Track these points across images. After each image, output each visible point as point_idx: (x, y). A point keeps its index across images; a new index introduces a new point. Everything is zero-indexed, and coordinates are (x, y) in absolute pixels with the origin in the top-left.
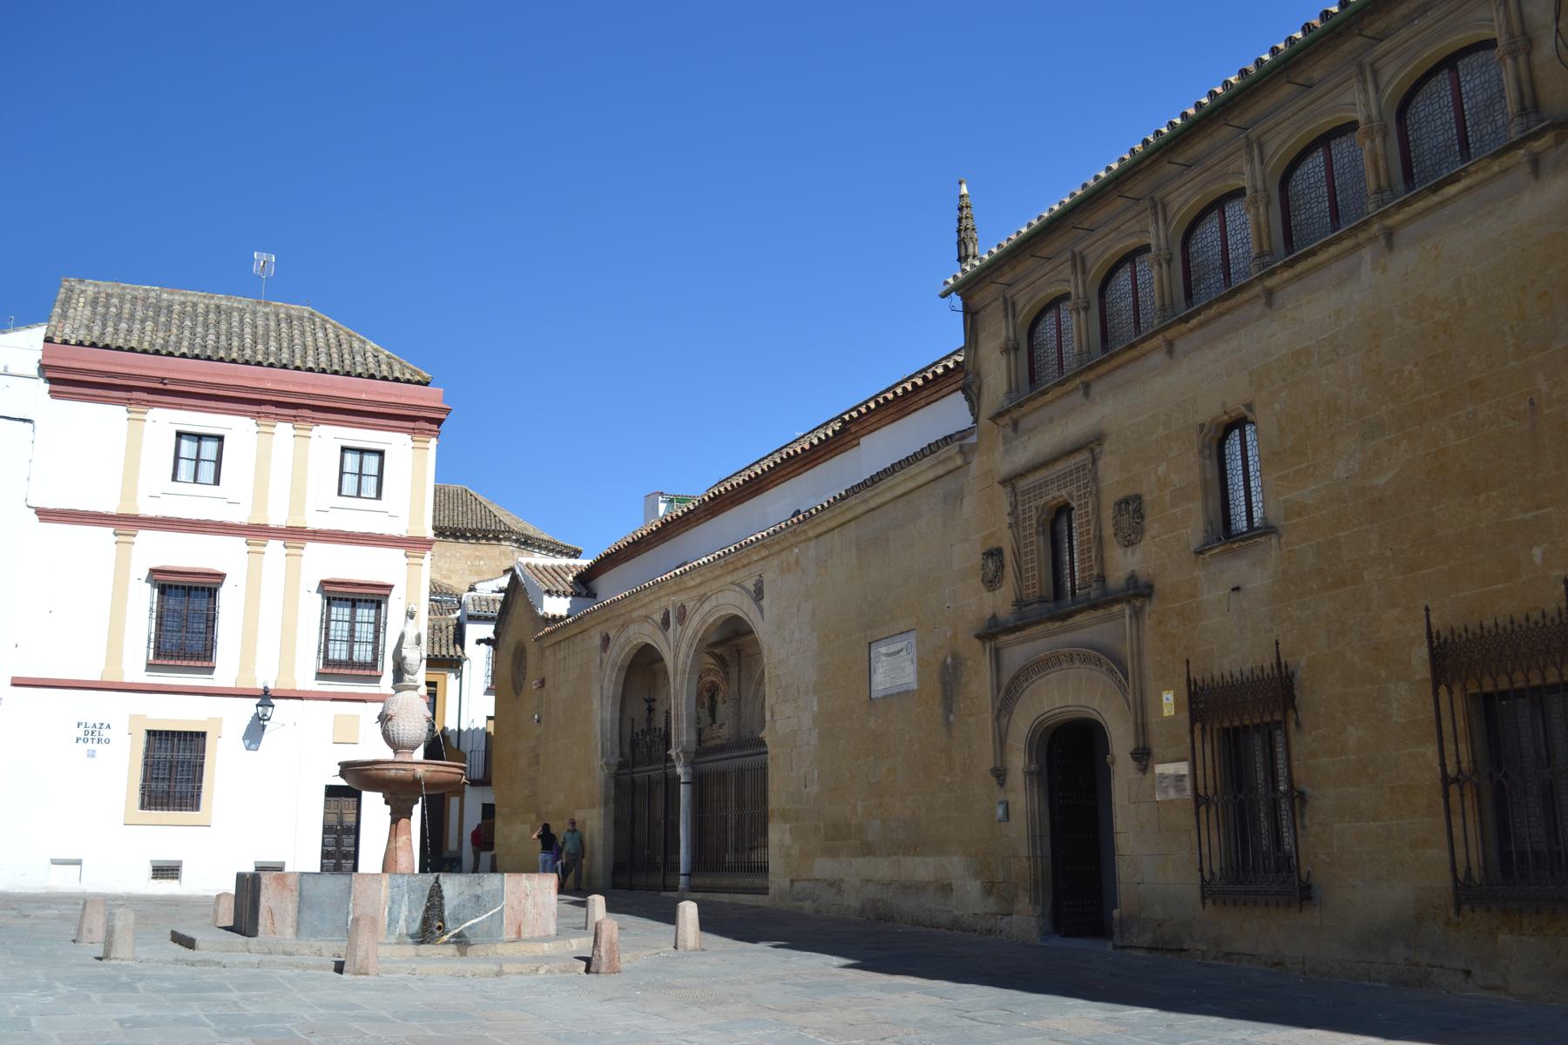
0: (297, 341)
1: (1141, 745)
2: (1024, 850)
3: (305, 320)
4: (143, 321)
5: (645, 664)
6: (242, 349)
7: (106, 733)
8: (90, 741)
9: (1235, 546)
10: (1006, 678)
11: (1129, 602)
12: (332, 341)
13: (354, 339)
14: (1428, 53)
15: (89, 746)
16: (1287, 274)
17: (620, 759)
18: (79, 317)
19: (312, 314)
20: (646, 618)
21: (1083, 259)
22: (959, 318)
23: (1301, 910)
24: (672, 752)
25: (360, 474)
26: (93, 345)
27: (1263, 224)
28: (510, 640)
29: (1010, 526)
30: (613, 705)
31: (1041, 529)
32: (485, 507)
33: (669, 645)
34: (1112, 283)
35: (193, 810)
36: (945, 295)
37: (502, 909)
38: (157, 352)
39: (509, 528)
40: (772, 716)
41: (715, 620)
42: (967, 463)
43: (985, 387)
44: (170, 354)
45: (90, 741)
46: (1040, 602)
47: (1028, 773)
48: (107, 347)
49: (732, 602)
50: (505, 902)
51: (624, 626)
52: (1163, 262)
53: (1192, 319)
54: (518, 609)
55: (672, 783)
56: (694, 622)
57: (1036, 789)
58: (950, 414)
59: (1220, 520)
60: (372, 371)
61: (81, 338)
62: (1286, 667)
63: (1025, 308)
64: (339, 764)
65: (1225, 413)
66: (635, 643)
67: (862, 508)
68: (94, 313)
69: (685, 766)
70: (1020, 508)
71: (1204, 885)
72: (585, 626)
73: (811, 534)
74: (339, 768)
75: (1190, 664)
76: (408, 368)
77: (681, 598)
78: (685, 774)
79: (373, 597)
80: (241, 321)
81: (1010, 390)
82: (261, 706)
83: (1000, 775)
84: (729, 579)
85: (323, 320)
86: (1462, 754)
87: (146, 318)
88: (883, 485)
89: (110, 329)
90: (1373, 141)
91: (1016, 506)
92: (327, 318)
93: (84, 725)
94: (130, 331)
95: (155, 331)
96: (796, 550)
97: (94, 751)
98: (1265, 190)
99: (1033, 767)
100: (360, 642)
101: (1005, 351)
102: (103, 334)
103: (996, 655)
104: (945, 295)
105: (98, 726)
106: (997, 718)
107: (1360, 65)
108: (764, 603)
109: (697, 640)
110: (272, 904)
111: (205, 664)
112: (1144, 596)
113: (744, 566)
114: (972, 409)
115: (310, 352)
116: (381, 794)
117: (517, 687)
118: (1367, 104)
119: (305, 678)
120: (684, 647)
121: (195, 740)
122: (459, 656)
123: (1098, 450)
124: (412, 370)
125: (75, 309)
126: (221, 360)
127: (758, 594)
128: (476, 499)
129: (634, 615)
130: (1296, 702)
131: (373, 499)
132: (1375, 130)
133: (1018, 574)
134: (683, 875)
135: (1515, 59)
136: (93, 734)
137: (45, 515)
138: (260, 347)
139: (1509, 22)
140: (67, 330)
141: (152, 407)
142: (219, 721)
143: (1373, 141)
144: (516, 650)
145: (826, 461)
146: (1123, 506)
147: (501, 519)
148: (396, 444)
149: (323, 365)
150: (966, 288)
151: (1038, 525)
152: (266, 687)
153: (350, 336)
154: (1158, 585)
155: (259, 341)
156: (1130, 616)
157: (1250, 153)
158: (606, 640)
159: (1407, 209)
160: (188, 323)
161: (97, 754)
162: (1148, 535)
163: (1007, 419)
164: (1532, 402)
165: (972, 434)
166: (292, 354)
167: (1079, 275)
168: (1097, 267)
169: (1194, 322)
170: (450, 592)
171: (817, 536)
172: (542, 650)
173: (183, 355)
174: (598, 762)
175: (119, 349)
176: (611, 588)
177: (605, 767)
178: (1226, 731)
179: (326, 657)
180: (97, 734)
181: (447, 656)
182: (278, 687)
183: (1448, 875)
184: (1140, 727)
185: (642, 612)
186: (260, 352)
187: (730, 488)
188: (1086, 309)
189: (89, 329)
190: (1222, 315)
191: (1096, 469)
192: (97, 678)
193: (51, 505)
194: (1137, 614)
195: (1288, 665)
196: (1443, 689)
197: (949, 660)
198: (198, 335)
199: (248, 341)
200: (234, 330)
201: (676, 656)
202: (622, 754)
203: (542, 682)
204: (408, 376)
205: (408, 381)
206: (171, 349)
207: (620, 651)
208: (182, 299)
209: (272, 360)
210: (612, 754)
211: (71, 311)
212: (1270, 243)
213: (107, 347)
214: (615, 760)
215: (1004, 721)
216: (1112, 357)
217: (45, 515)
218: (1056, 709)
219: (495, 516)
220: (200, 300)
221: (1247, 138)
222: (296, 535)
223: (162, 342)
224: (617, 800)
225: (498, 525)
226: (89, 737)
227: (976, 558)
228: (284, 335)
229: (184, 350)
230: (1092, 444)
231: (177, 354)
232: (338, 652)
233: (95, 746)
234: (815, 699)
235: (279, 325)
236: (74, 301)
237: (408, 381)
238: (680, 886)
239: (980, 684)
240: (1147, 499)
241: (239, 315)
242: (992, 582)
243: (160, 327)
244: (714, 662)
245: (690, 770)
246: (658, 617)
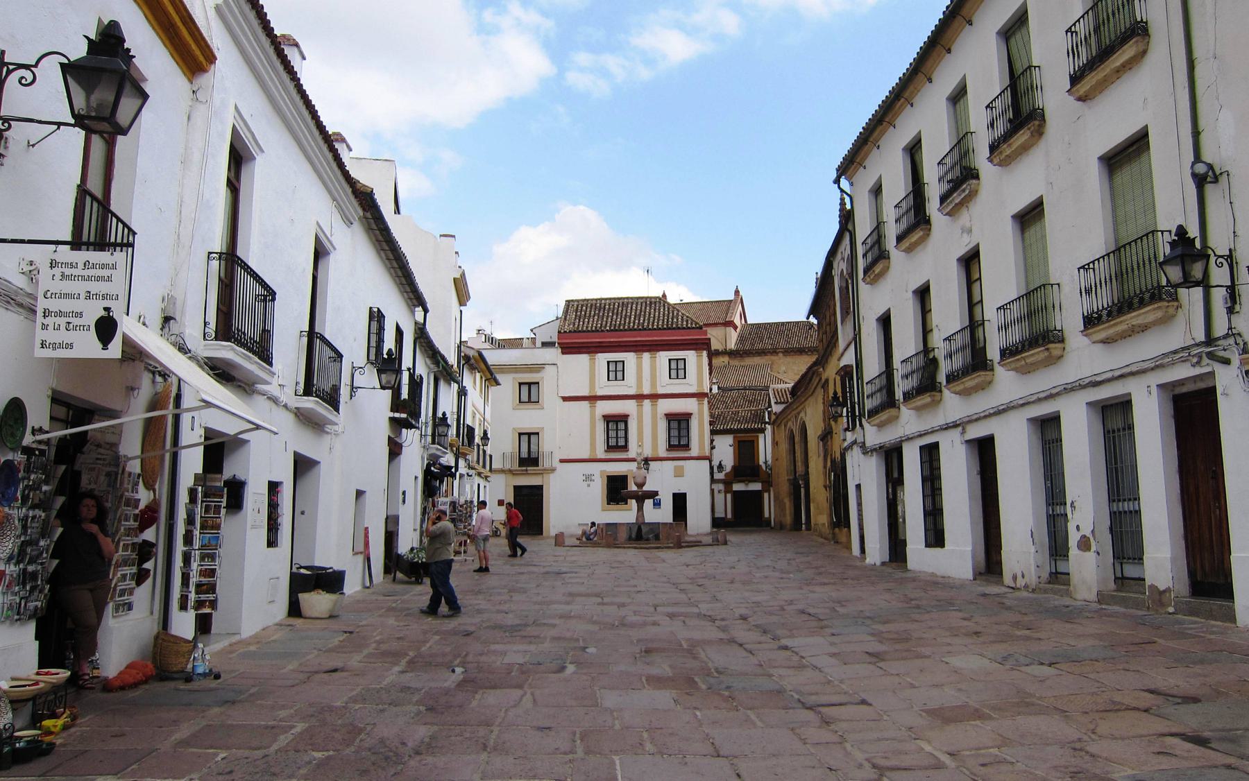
7: (593, 478)
15: (588, 482)
23: (235, 475)
25: (677, 369)
79: (623, 419)
95: (569, 325)
115: (656, 320)
119: (662, 452)
137: (565, 399)
148: (690, 356)
179: (608, 443)
192: (687, 461)
199: (680, 320)
217: (565, 399)
222: (654, 397)
232: (612, 442)
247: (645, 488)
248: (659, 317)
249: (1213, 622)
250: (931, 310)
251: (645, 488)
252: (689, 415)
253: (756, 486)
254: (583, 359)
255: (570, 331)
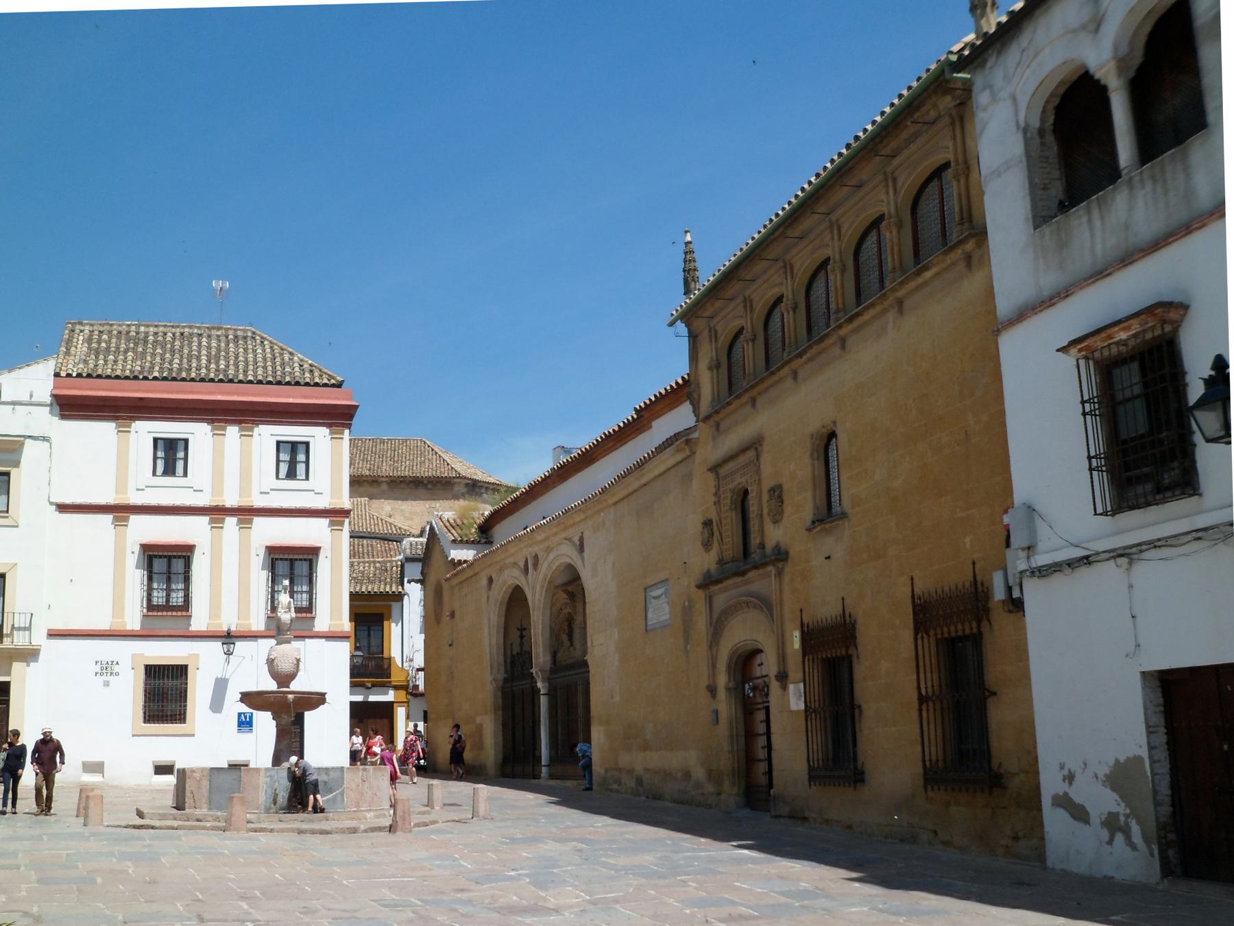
0: (241, 358)
1: (782, 669)
2: (726, 746)
3: (249, 339)
4: (126, 352)
5: (516, 600)
6: (198, 369)
7: (116, 668)
8: (105, 674)
9: (827, 526)
10: (715, 616)
11: (774, 565)
12: (269, 355)
13: (286, 352)
14: (921, 168)
15: (104, 678)
16: (850, 327)
17: (506, 676)
18: (78, 353)
19: (254, 333)
20: (515, 564)
21: (751, 301)
22: (684, 343)
24: (533, 671)
26: (89, 376)
27: (839, 288)
28: (432, 579)
29: (715, 503)
30: (498, 632)
31: (733, 506)
32: (440, 456)
33: (528, 585)
34: (771, 320)
35: (181, 723)
36: (671, 324)
37: (343, 790)
38: (136, 378)
39: (459, 474)
40: (592, 643)
41: (558, 567)
42: (693, 453)
43: (702, 395)
44: (145, 378)
45: (105, 674)
46: (733, 561)
47: (728, 689)
48: (99, 376)
49: (569, 553)
50: (345, 786)
51: (501, 570)
52: (790, 309)
53: (804, 355)
54: (436, 556)
55: (535, 692)
56: (544, 568)
57: (733, 701)
58: (681, 418)
59: (825, 506)
60: (297, 379)
61: (80, 371)
62: (850, 616)
63: (724, 337)
64: (240, 693)
65: (824, 427)
66: (509, 583)
67: (636, 485)
68: (89, 348)
69: (543, 682)
70: (721, 489)
71: (811, 769)
72: (476, 571)
73: (611, 502)
74: (240, 696)
75: (803, 612)
76: (326, 373)
77: (535, 549)
78: (543, 687)
80: (200, 343)
81: (713, 401)
82: (225, 644)
83: (712, 690)
84: (563, 535)
85: (262, 337)
86: (931, 682)
87: (128, 349)
88: (647, 467)
89: (101, 362)
90: (891, 232)
91: (719, 488)
92: (265, 336)
93: (100, 663)
94: (115, 362)
96: (602, 514)
97: (108, 682)
98: (841, 261)
99: (731, 685)
100: (302, 591)
101: (710, 369)
102: (96, 366)
103: (710, 600)
104: (671, 324)
105: (110, 663)
106: (711, 647)
107: (885, 173)
108: (586, 554)
109: (547, 582)
110: (192, 788)
111: (184, 613)
112: (782, 560)
113: (572, 526)
114: (694, 411)
115: (251, 367)
116: (270, 713)
117: (438, 619)
118: (889, 203)
120: (538, 589)
121: (179, 672)
122: (400, 592)
123: (759, 449)
124: (329, 375)
125: (76, 348)
126: (183, 380)
127: (581, 549)
128: (433, 450)
129: (507, 561)
130: (857, 641)
131: (303, 480)
132: (891, 224)
133: (720, 540)
134: (545, 766)
135: (959, 181)
136: (107, 669)
137: (63, 508)
138: (213, 366)
139: (956, 150)
140: (70, 366)
141: (134, 420)
142: (197, 656)
143: (891, 232)
144: (436, 588)
145: (633, 438)
146: (772, 492)
147: (453, 466)
148: (318, 436)
149: (260, 378)
150: (688, 316)
151: (732, 503)
152: (229, 630)
153: (282, 349)
154: (792, 553)
155: (212, 361)
156: (775, 575)
157: (832, 232)
158: (491, 580)
159: (906, 286)
160: (159, 351)
161: (111, 684)
162: (786, 514)
163: (711, 422)
164: (966, 434)
165: (696, 431)
166: (236, 370)
167: (748, 314)
168: (760, 308)
169: (805, 358)
170: (408, 533)
171: (616, 503)
172: (452, 588)
173: (155, 378)
174: (489, 678)
175: (108, 377)
176: (504, 532)
177: (493, 682)
178: (823, 660)
179: (149, 600)
180: (109, 669)
181: (390, 593)
182: (238, 629)
183: (920, 764)
184: (781, 656)
185: (511, 560)
186: (213, 370)
187: (570, 460)
188: (753, 340)
189: (86, 362)
190: (820, 353)
191: (760, 464)
193: (68, 501)
194: (780, 574)
195: (852, 615)
196: (919, 636)
197: (687, 603)
198: (166, 360)
200: (193, 353)
201: (534, 595)
202: (506, 672)
203: (452, 615)
204: (326, 381)
205: (325, 385)
206: (146, 374)
207: (500, 592)
208: (156, 330)
209: (221, 377)
210: (499, 670)
211: (73, 348)
212: (844, 303)
213: (99, 376)
214: (501, 676)
215: (714, 650)
216: (773, 373)
217: (63, 508)
218: (748, 640)
219: (448, 464)
220: (168, 329)
221: (830, 220)
222: (246, 513)
223: (139, 368)
224: (504, 708)
225: (450, 472)
226: (104, 671)
227: (700, 527)
228: (231, 354)
229: (156, 374)
230: (755, 445)
231: (150, 377)
233: (109, 678)
234: (616, 630)
235: (228, 345)
236: (75, 340)
237: (325, 385)
238: (542, 775)
239: (701, 623)
240: (785, 488)
241: (198, 340)
242: (707, 545)
243: (139, 356)
244: (567, 597)
245: (547, 685)
246: (522, 564)
247: (295, 686)
248: (256, 362)
249: (723, 852)
250: (1218, 211)
251: (295, 686)
252: (315, 551)
253: (390, 696)
254: (103, 431)
255: (79, 375)
